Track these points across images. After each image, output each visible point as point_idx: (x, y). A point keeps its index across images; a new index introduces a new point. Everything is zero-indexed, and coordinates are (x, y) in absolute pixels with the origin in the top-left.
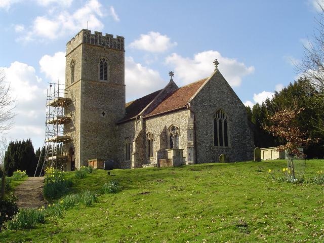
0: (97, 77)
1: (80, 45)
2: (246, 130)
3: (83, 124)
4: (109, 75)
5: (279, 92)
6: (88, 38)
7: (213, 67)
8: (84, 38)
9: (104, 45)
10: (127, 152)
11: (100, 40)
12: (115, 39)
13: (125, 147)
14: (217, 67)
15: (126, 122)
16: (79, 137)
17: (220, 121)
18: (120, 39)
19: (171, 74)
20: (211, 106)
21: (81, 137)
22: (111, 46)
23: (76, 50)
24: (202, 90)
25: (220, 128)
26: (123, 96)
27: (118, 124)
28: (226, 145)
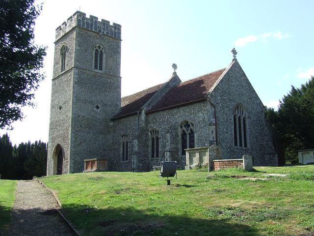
0: (91, 66)
1: (73, 29)
3: (75, 118)
4: (104, 65)
7: (231, 57)
8: (78, 21)
9: (100, 31)
10: (123, 152)
11: (96, 25)
12: (111, 26)
13: (121, 146)
14: (235, 56)
15: (123, 117)
16: (70, 132)
17: (239, 118)
19: (175, 66)
20: (230, 100)
21: (72, 132)
24: (222, 81)
25: (239, 125)
27: (112, 120)
28: (246, 146)
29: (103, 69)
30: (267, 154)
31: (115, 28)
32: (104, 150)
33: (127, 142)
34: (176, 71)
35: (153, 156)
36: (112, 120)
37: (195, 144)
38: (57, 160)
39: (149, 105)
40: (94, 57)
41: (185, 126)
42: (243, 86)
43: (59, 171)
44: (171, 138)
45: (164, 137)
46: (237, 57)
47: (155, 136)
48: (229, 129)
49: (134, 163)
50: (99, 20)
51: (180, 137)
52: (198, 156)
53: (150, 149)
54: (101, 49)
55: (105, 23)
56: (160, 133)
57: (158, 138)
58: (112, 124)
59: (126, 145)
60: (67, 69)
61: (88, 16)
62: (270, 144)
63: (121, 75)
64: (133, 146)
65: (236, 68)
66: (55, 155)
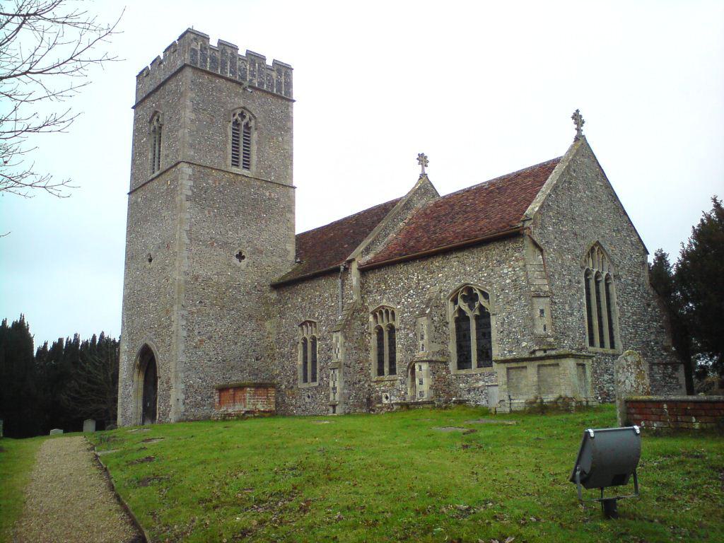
0: (225, 159)
4: (254, 158)
9: (244, 78)
11: (233, 65)
12: (268, 68)
13: (300, 346)
18: (283, 71)
22: (261, 84)
23: (167, 87)
26: (288, 215)
28: (612, 346)
29: (253, 168)
31: (279, 72)
33: (314, 340)
34: (427, 170)
35: (381, 372)
36: (277, 287)
39: (367, 250)
40: (230, 138)
41: (464, 298)
44: (429, 326)
46: (586, 131)
47: (384, 325)
48: (575, 305)
49: (334, 388)
51: (452, 326)
52: (535, 379)
53: (373, 356)
54: (245, 121)
55: (255, 59)
56: (398, 317)
57: (392, 330)
58: (274, 296)
59: (310, 346)
60: (163, 166)
61: (213, 43)
65: (581, 147)
66: (137, 370)
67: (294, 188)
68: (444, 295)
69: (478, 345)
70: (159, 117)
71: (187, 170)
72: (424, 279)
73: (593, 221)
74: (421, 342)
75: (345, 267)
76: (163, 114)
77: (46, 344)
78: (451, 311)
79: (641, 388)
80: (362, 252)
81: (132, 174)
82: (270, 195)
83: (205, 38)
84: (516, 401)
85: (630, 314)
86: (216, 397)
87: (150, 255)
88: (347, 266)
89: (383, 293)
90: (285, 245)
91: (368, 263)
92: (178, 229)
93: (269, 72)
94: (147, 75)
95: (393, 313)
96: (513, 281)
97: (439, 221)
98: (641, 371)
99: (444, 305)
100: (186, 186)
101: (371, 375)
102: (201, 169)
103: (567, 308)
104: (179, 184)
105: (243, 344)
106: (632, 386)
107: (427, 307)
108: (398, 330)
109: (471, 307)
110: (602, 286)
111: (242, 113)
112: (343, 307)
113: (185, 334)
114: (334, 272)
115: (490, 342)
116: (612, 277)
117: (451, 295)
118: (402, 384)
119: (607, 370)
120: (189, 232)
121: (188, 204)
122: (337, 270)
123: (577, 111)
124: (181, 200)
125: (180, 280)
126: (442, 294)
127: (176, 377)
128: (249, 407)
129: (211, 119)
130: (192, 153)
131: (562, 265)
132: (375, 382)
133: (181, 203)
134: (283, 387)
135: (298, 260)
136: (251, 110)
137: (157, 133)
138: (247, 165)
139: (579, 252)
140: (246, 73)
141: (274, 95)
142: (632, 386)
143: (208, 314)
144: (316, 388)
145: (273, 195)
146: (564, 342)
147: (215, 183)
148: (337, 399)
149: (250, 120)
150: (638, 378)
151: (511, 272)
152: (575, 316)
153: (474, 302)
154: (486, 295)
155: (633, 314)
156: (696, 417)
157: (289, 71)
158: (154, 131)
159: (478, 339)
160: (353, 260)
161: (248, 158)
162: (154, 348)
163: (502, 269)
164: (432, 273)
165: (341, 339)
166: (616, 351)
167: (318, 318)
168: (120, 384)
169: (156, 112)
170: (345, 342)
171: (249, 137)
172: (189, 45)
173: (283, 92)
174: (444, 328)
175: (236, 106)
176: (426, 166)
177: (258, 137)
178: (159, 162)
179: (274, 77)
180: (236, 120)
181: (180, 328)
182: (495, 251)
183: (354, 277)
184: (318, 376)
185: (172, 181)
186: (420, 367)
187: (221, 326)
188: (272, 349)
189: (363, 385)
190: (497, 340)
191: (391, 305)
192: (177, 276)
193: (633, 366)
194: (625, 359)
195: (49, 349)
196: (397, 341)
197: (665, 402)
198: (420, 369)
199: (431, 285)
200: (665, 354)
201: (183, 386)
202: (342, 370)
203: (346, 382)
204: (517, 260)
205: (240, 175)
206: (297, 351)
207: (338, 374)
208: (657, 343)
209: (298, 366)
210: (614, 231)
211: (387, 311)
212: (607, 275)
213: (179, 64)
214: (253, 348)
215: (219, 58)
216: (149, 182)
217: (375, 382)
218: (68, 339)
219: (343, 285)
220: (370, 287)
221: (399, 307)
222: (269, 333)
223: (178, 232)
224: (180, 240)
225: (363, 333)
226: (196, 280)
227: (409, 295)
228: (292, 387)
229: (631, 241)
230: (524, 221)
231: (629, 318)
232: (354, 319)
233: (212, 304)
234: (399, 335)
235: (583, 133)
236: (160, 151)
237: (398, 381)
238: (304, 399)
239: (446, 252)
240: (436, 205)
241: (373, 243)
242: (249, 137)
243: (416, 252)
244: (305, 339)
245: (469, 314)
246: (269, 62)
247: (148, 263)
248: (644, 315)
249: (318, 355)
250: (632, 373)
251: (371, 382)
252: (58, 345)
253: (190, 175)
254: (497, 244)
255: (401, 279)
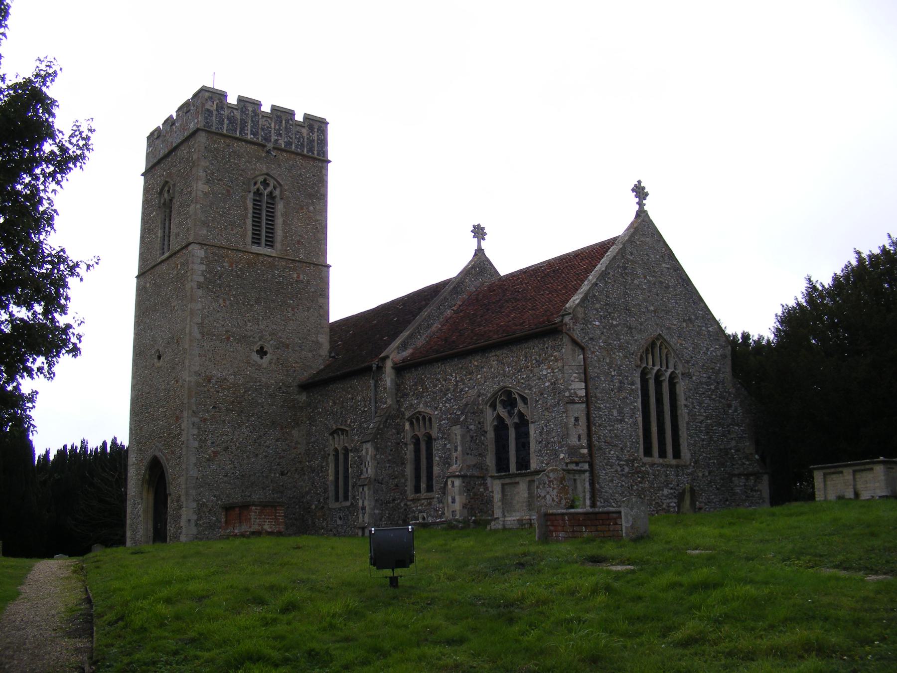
0: (243, 236)
2: (730, 406)
4: (279, 233)
5: (827, 286)
6: (219, 115)
9: (267, 139)
11: (255, 124)
12: (298, 124)
19: (479, 232)
22: (289, 144)
23: (179, 153)
26: (321, 300)
28: (677, 454)
29: (278, 245)
30: (739, 475)
31: (311, 128)
32: (282, 474)
33: (346, 450)
34: (484, 245)
35: (417, 490)
36: (306, 387)
37: (532, 455)
38: (151, 504)
39: (404, 346)
40: (251, 211)
41: (503, 403)
42: (667, 287)
43: (160, 535)
44: (463, 437)
45: (446, 435)
46: (650, 206)
47: (421, 433)
48: (627, 410)
49: (364, 508)
50: (263, 109)
51: (491, 435)
52: (526, 495)
53: (409, 470)
54: (269, 189)
55: (282, 115)
56: (435, 425)
57: (429, 440)
58: (303, 397)
59: (342, 457)
60: (175, 246)
61: (232, 100)
62: (748, 445)
63: (329, 261)
64: (361, 460)
66: (146, 486)
67: (329, 266)
68: (483, 400)
69: (517, 457)
70: (170, 188)
71: (198, 252)
72: (462, 380)
73: (655, 311)
74: (455, 455)
75: (377, 365)
76: (174, 185)
77: (47, 452)
78: (489, 416)
79: (564, 502)
80: (398, 347)
81: (141, 254)
82: (298, 277)
83: (223, 95)
84: (510, 519)
85: (702, 418)
86: (223, 516)
87: (158, 350)
88: (380, 365)
89: (419, 396)
90: (317, 337)
91: (404, 361)
92: (188, 321)
93: (298, 128)
94: (158, 137)
95: (430, 419)
96: (551, 384)
97: (488, 310)
98: (565, 486)
99: (482, 411)
100: (197, 271)
101: (408, 492)
102: (215, 250)
103: (615, 413)
104: (190, 268)
105: (266, 456)
106: (553, 500)
107: (462, 414)
108: (435, 440)
109: (510, 414)
110: (665, 387)
111: (265, 180)
112: (376, 413)
113: (196, 444)
114: (366, 371)
115: (529, 454)
116: (680, 376)
117: (490, 399)
118: (439, 503)
119: (668, 484)
120: (201, 325)
121: (200, 292)
122: (370, 368)
123: (639, 182)
124: (192, 288)
125: (190, 382)
126: (481, 399)
127: (187, 494)
128: (255, 528)
129: (228, 191)
130: (205, 232)
131: (610, 365)
132: (411, 500)
133: (192, 291)
134: (313, 507)
135: (333, 355)
136: (276, 176)
137: (167, 206)
138: (270, 243)
139: (633, 348)
140: (270, 132)
141: (304, 156)
142: (553, 500)
143: (224, 421)
144: (348, 507)
145: (301, 277)
146: (610, 453)
147: (231, 266)
148: (366, 520)
149: (275, 188)
150: (561, 493)
151: (550, 373)
152: (627, 423)
153: (513, 408)
154: (524, 399)
155: (707, 418)
156: (585, 526)
157: (323, 125)
158: (164, 204)
159: (517, 451)
160: (387, 357)
161: (272, 233)
162: (163, 461)
163: (541, 371)
164: (470, 374)
165: (371, 451)
166: (681, 462)
167: (350, 425)
168: (128, 502)
169: (167, 182)
170: (376, 455)
171: (273, 208)
172: (203, 105)
173: (316, 152)
174: (483, 438)
175: (257, 173)
176: (484, 239)
177: (284, 207)
178: (169, 241)
179: (305, 135)
180: (258, 190)
181: (191, 437)
182: (534, 349)
183: (388, 377)
184: (350, 494)
185: (183, 265)
186: (453, 483)
187: (239, 435)
188: (300, 462)
189: (399, 504)
190: (535, 451)
191: (429, 410)
192: (187, 377)
193: (555, 482)
194: (546, 475)
195: (52, 458)
196: (434, 452)
197: (566, 514)
198: (453, 486)
199: (469, 388)
200: (747, 463)
201: (194, 505)
202: (372, 487)
203: (376, 501)
204: (556, 360)
205: (261, 254)
206: (328, 464)
207: (367, 492)
208: (737, 451)
209: (328, 483)
210: (684, 321)
211: (424, 418)
212: (673, 373)
213: (192, 126)
214: (277, 460)
215: (239, 118)
216: (158, 264)
217: (411, 500)
218: (72, 447)
219: (376, 387)
220: (406, 389)
221: (436, 413)
222: (297, 443)
223: (188, 326)
224: (190, 335)
225: (399, 444)
226: (209, 381)
227: (447, 399)
228: (323, 507)
229: (709, 331)
230: (563, 316)
231: (701, 422)
232: (387, 428)
233: (227, 409)
234: (437, 445)
235: (646, 208)
236: (170, 228)
237: (435, 500)
238: (336, 520)
239: (484, 350)
240: (491, 288)
241: (411, 336)
242: (273, 208)
243: (454, 349)
244: (336, 450)
245: (508, 421)
246: (299, 117)
247: (156, 360)
248: (723, 419)
249: (350, 470)
250: (554, 488)
251: (408, 500)
252: (61, 453)
253: (202, 259)
254: (537, 342)
255: (438, 380)
